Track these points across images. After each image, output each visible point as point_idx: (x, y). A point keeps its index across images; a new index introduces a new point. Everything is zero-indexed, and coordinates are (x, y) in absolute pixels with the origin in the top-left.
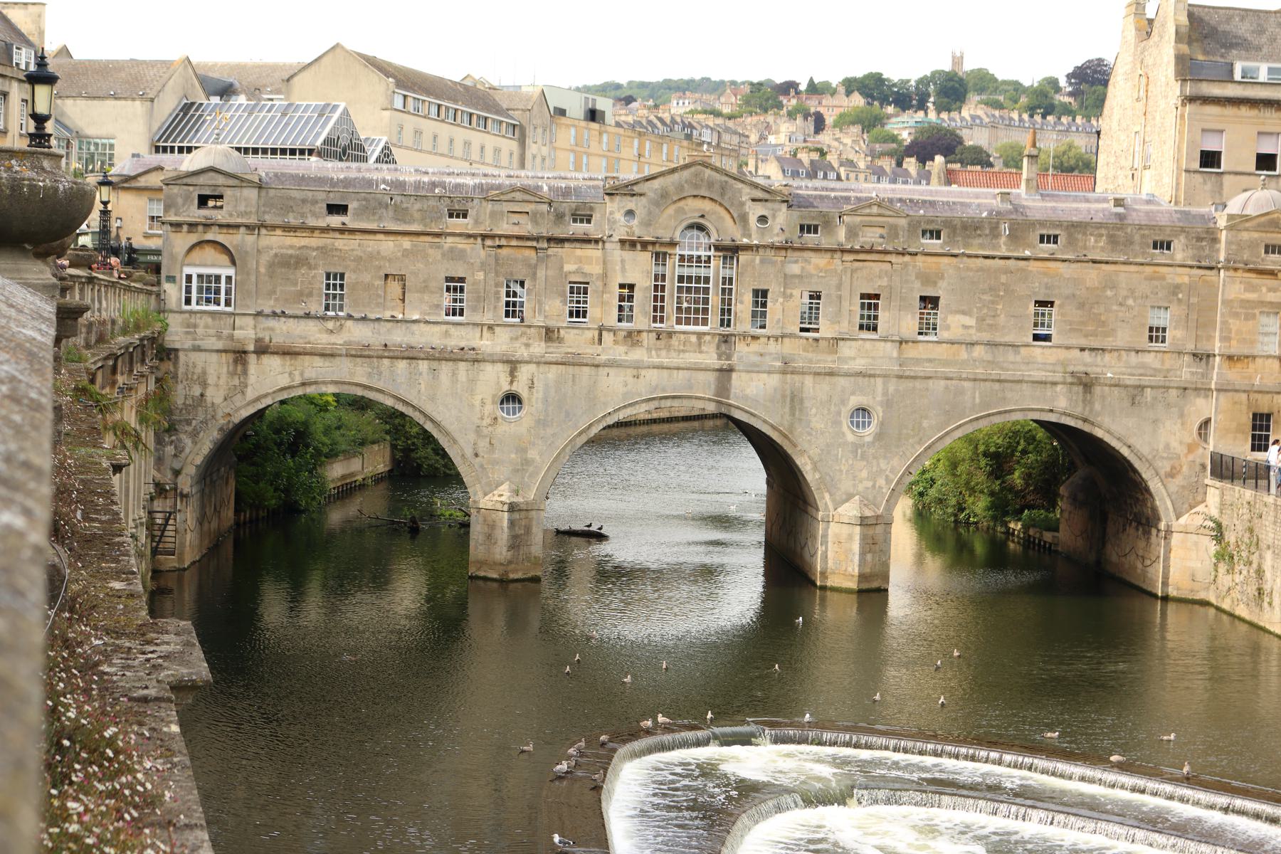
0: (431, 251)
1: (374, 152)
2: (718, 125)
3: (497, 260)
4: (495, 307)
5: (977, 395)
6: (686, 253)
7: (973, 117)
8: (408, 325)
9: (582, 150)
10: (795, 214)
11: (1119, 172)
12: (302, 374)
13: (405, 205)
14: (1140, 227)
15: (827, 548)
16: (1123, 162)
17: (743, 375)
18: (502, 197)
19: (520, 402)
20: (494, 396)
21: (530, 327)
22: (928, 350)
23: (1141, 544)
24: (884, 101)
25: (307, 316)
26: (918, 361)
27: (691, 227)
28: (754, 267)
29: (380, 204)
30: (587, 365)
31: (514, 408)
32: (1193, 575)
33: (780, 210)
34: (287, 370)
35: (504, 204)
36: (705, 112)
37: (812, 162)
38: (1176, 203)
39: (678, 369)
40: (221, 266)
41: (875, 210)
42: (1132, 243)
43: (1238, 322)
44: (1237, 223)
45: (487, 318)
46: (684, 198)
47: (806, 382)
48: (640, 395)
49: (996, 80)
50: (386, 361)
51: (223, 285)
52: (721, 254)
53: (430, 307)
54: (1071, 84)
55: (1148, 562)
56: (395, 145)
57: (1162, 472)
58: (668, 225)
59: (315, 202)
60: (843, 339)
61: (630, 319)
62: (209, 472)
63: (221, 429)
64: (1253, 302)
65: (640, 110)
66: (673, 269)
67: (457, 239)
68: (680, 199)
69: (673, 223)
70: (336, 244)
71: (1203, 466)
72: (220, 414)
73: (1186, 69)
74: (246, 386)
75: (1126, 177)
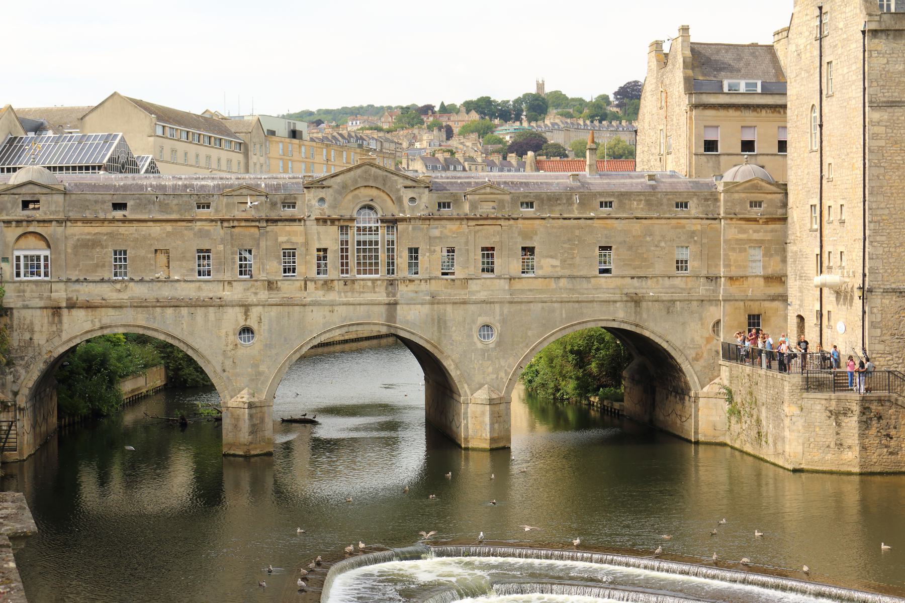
0: (185, 232)
2: (380, 137)
3: (232, 236)
4: (232, 269)
5: (564, 312)
6: (361, 225)
7: (553, 124)
8: (173, 283)
9: (288, 158)
11: (651, 157)
12: (100, 321)
13: (166, 202)
14: (667, 193)
15: (467, 422)
16: (653, 150)
17: (405, 306)
18: (233, 193)
19: (252, 333)
20: (234, 330)
21: (256, 281)
22: (527, 283)
23: (679, 407)
24: (492, 116)
25: (102, 281)
26: (522, 291)
27: (364, 207)
29: (149, 201)
32: (714, 426)
34: (90, 318)
36: (371, 129)
37: (446, 159)
38: (690, 176)
39: (360, 304)
40: (40, 249)
41: (488, 190)
42: (661, 205)
43: (735, 254)
44: (731, 187)
45: (227, 276)
47: (448, 309)
49: (567, 98)
50: (158, 309)
51: (42, 262)
52: (385, 225)
54: (617, 99)
55: (684, 419)
56: (158, 161)
57: (690, 358)
58: (348, 208)
59: (104, 202)
61: (325, 272)
62: (38, 392)
63: (45, 362)
65: (326, 130)
66: (353, 236)
70: (120, 230)
71: (717, 352)
72: (44, 351)
73: (692, 86)
74: (62, 331)
75: (656, 160)
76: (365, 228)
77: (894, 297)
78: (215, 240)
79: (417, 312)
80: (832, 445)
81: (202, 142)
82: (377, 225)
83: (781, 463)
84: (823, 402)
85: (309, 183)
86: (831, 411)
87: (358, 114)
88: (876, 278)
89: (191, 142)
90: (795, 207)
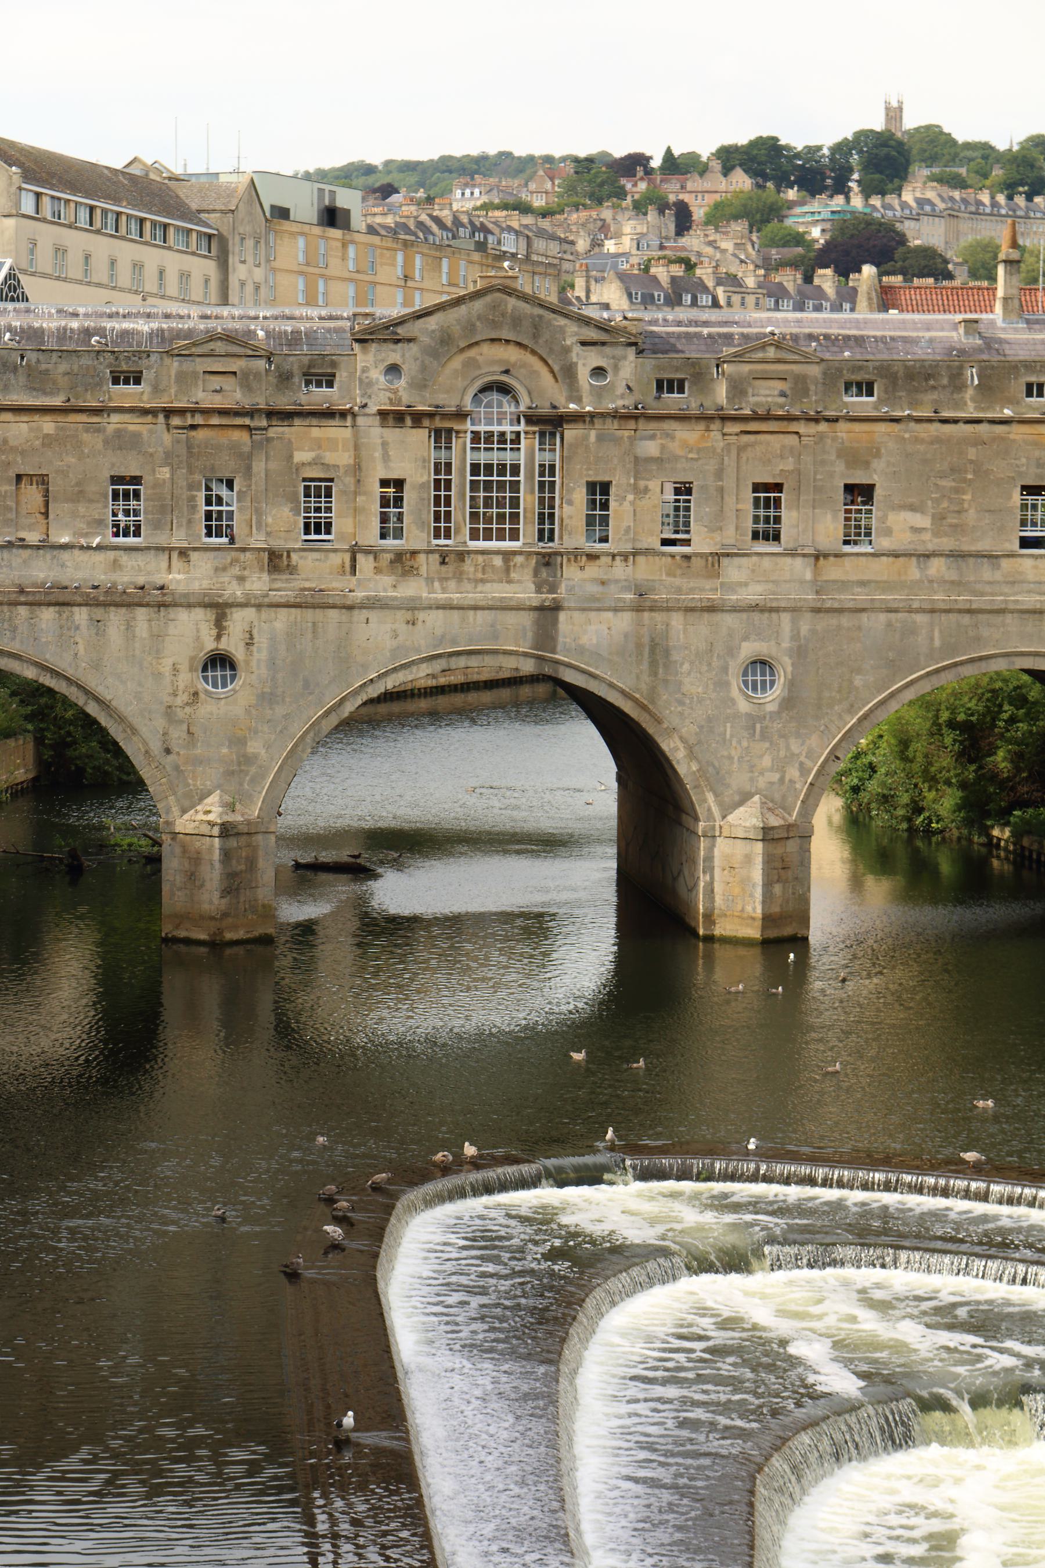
0: (86, 437)
2: (526, 226)
3: (189, 447)
6: (482, 428)
7: (921, 202)
8: (55, 552)
10: (649, 363)
13: (43, 367)
17: (576, 614)
18: (194, 350)
20: (192, 659)
24: (783, 181)
26: (844, 585)
28: (587, 447)
33: (625, 358)
35: (198, 359)
36: (505, 207)
37: (674, 279)
39: (476, 608)
41: (771, 353)
45: (178, 539)
46: (477, 343)
47: (674, 623)
48: (418, 650)
49: (954, 142)
52: (536, 429)
53: (89, 524)
56: (24, 272)
60: (728, 555)
61: (399, 534)
67: (126, 417)
68: (470, 346)
69: (460, 383)
76: (489, 435)
78: (151, 455)
79: (604, 627)
82: (516, 428)
85: (364, 331)
87: (477, 172)
89: (98, 232)
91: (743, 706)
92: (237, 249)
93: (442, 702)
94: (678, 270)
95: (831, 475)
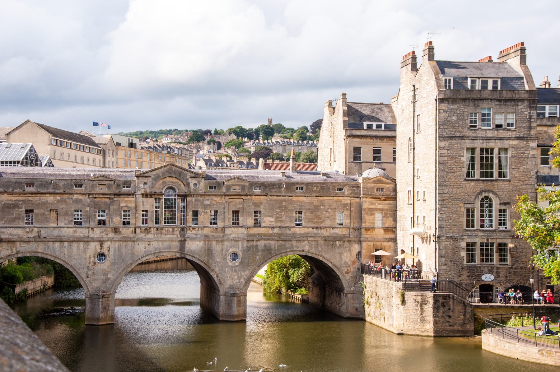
0: (68, 200)
1: (44, 163)
2: (181, 147)
3: (94, 203)
6: (167, 198)
7: (277, 142)
9: (128, 158)
10: (207, 182)
11: (325, 163)
12: (16, 249)
13: (57, 183)
17: (190, 243)
18: (96, 179)
20: (94, 255)
24: (243, 136)
26: (254, 235)
27: (168, 188)
30: (130, 241)
31: (102, 259)
36: (176, 143)
37: (217, 160)
38: (346, 174)
39: (165, 241)
41: (236, 180)
42: (329, 189)
44: (366, 180)
45: (92, 224)
47: (213, 244)
49: (285, 128)
53: (68, 222)
54: (312, 129)
55: (340, 305)
56: (53, 159)
57: (344, 272)
58: (159, 187)
61: (146, 223)
64: (373, 209)
65: (151, 142)
67: (78, 195)
68: (164, 178)
69: (162, 187)
71: (358, 269)
77: (452, 241)
79: (196, 245)
80: (419, 321)
81: (78, 148)
83: (391, 330)
84: (414, 297)
86: (418, 302)
87: (169, 134)
88: (442, 230)
89: (72, 149)
90: (400, 192)
91: (230, 264)
92: (108, 153)
93: (159, 265)
94: (218, 158)
95: (251, 209)
